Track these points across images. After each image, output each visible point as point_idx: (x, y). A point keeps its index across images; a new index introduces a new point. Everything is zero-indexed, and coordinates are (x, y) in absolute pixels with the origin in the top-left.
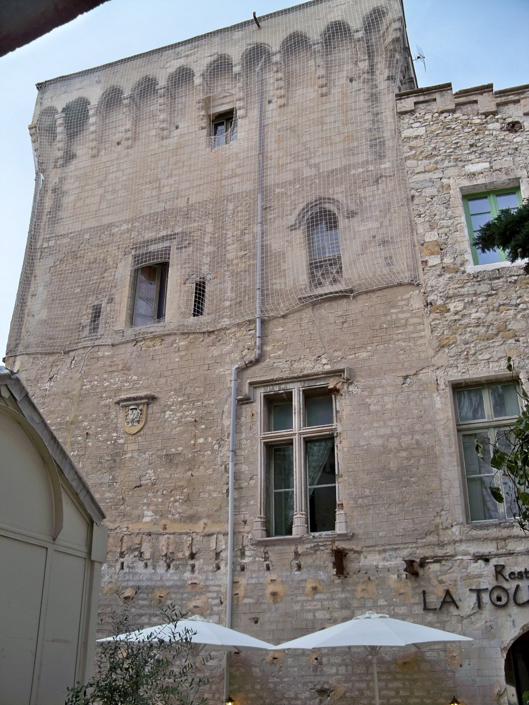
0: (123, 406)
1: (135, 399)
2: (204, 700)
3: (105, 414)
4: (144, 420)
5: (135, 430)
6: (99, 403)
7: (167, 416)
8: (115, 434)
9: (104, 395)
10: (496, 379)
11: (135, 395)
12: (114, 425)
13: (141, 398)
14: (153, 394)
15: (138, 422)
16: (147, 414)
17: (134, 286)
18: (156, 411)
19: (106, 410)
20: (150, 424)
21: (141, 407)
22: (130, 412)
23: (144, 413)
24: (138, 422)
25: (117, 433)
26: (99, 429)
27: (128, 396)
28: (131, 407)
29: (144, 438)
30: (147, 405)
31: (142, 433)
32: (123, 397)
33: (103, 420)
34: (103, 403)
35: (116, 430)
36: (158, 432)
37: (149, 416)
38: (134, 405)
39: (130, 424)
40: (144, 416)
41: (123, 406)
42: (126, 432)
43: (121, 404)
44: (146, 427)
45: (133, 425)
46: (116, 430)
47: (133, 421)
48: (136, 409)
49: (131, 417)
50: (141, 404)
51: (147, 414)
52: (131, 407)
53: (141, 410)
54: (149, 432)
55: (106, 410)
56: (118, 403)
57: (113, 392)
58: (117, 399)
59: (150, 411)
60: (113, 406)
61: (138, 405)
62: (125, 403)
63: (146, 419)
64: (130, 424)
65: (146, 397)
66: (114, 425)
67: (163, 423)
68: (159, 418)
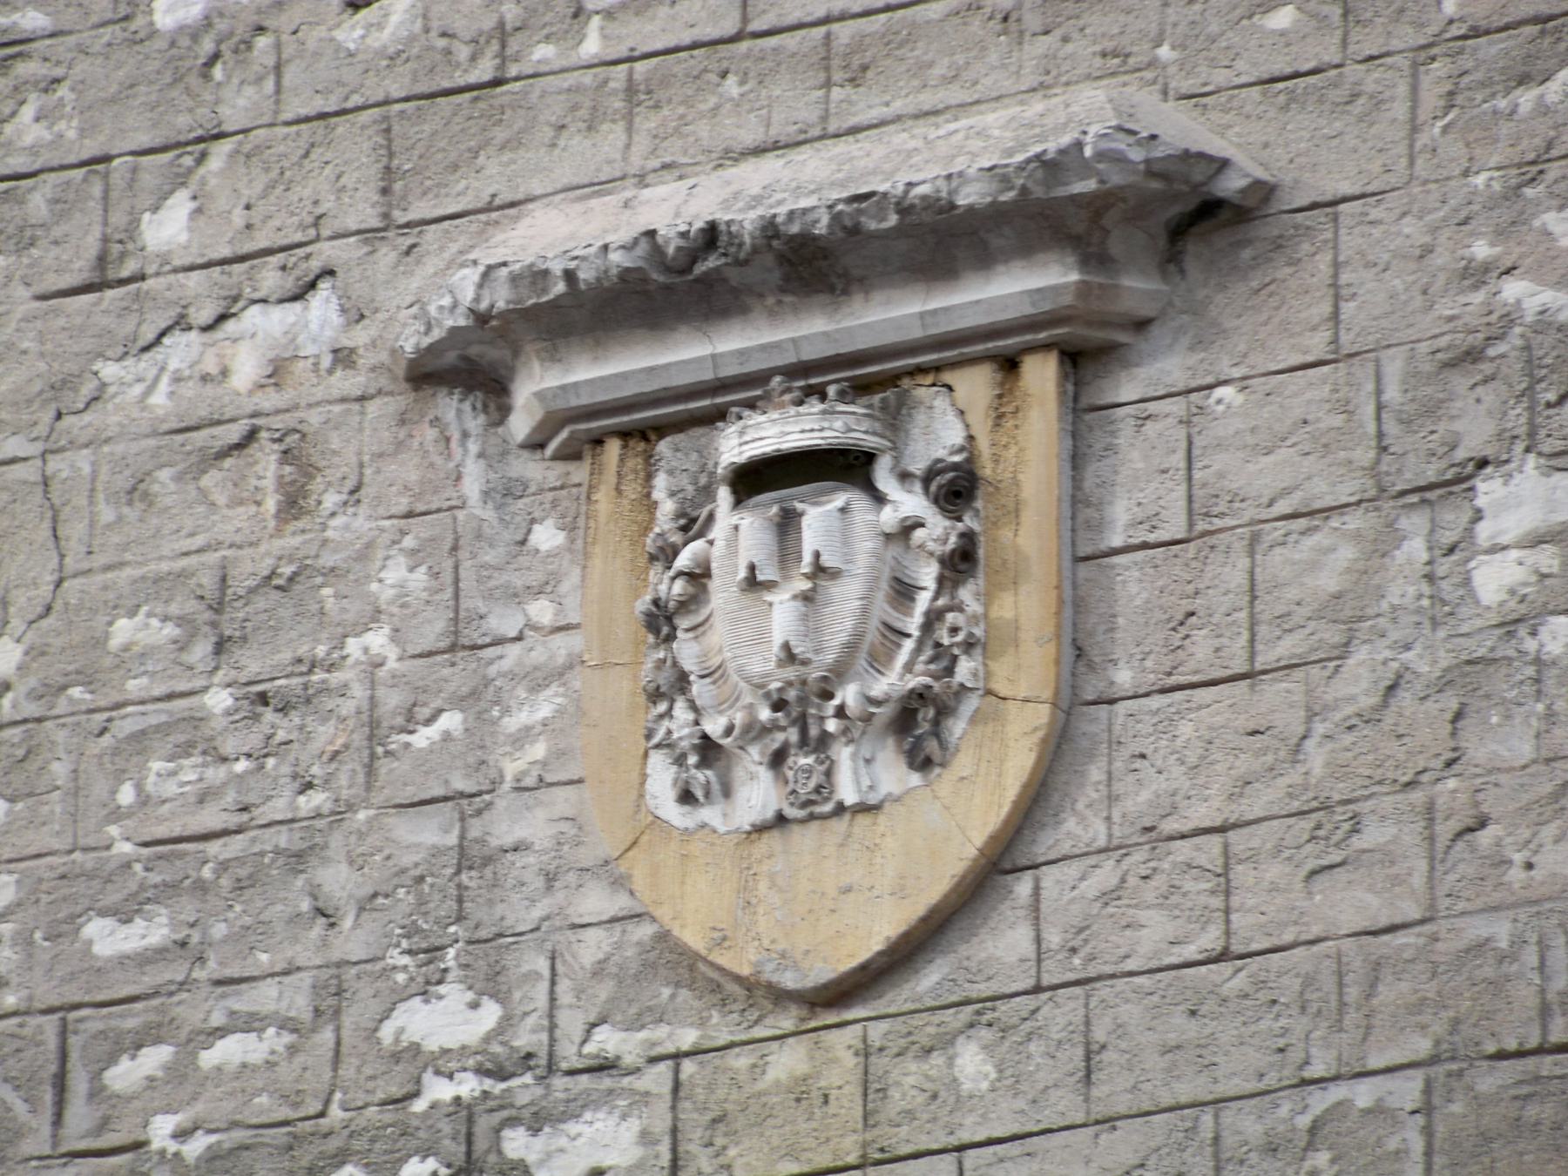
0: (580, 433)
1: (808, 262)
2: (1266, 1172)
3: (219, 622)
4: (1026, 675)
5: (851, 900)
6: (66, 395)
7: (1495, 580)
8: (448, 1020)
9: (168, 228)
10: (924, 920)
11: (799, 186)
12: (430, 833)
13: (939, 238)
14: (1183, 130)
15: (917, 725)
16: (1085, 557)
17: (1028, 161)
18: (1259, 477)
19: (233, 520)
20: (1170, 759)
21: (941, 427)
22: (739, 534)
23: (1029, 534)
24: (917, 725)
25: (490, 983)
26: (107, 938)
27: (673, 209)
28: (736, 445)
29: (1051, 1066)
30: (1082, 360)
31: (1002, 945)
32: (569, 234)
33: (192, 738)
34: (148, 388)
35: (454, 924)
36: (1351, 903)
37: (1133, 587)
38: (806, 378)
39: (757, 793)
40: (1024, 607)
41: (580, 433)
42: (675, 962)
43: (538, 384)
44: (1078, 825)
45: (815, 807)
46: (454, 924)
47: (800, 715)
48: (845, 467)
49: (748, 640)
50: (939, 356)
51: (1085, 557)
52: (736, 445)
53: (956, 488)
54: (1154, 934)
55: (233, 520)
56: (465, 370)
57: (354, 147)
58: (444, 289)
59: (1141, 487)
60: (365, 435)
61: (879, 378)
62: (634, 363)
63: (1079, 653)
64: (757, 793)
65: (1038, 211)
66: (430, 833)
67: (1424, 718)
68: (1349, 616)
